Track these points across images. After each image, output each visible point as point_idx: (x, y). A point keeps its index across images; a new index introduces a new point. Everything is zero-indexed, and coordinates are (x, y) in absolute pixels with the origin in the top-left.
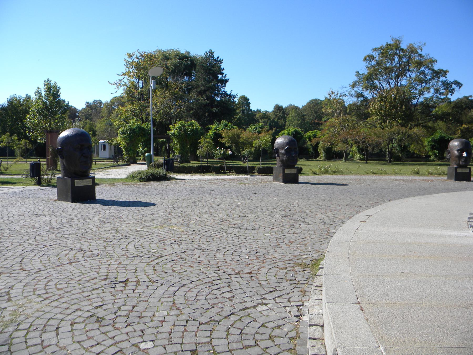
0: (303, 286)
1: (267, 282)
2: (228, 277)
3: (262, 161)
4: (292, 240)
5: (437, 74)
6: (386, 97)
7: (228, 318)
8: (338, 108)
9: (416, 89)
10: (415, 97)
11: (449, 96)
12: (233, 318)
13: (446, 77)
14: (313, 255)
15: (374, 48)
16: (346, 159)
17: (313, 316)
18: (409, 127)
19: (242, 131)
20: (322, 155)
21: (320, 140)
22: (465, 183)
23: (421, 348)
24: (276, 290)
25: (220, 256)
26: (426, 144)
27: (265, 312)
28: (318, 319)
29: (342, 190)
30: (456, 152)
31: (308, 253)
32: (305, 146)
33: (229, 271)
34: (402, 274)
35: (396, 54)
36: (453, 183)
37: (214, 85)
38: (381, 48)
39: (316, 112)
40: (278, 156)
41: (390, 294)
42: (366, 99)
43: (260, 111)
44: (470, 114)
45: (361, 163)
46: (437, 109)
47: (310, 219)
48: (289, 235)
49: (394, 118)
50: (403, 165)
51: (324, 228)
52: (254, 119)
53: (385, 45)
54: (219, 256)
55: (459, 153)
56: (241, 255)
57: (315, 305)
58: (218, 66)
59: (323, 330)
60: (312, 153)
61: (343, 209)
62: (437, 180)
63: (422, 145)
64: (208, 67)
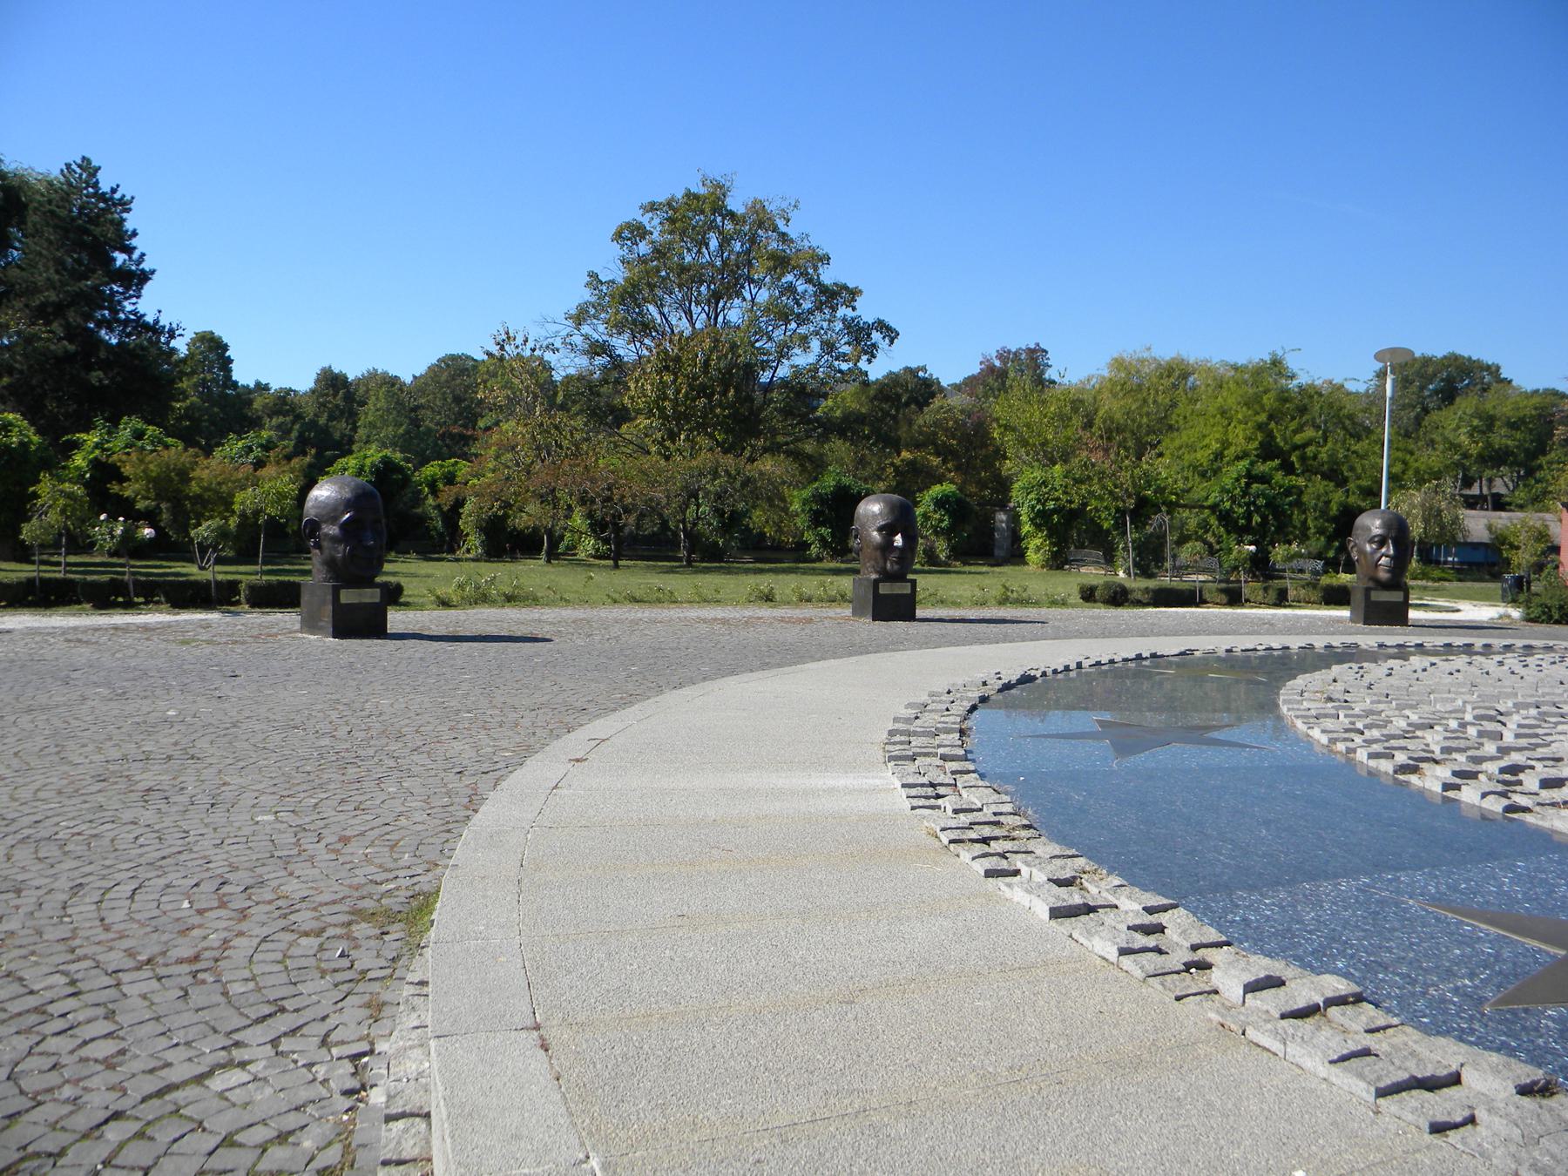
0: (376, 987)
1: (251, 985)
2: (108, 981)
3: (265, 562)
4: (348, 833)
5: (832, 296)
6: (677, 359)
7: (97, 1134)
8: (528, 387)
9: (770, 339)
10: (768, 361)
11: (863, 365)
12: (114, 1133)
13: (854, 309)
14: (415, 880)
15: (646, 201)
16: (552, 555)
17: (400, 1086)
18: (747, 453)
19: (196, 456)
20: (474, 541)
21: (468, 491)
22: (899, 626)
23: (709, 1143)
24: (283, 1010)
25: (83, 910)
26: (796, 506)
27: (238, 1091)
28: (416, 1091)
29: (529, 658)
30: (875, 533)
31: (401, 873)
32: (419, 510)
33: (115, 959)
34: (679, 921)
35: (712, 226)
36: (869, 628)
37: (96, 288)
38: (669, 204)
39: (458, 400)
40: (318, 546)
41: (636, 986)
42: (617, 363)
43: (266, 388)
44: (921, 421)
45: (598, 566)
46: (830, 403)
47: (415, 758)
48: (342, 817)
49: (702, 427)
50: (729, 571)
51: (461, 786)
52: (245, 417)
53: (679, 195)
54: (82, 908)
55: (884, 537)
56: (164, 899)
57: (411, 1048)
58: (112, 222)
59: (430, 1125)
60: (441, 535)
61: (526, 722)
62: (822, 619)
63: (786, 510)
64: (73, 219)
